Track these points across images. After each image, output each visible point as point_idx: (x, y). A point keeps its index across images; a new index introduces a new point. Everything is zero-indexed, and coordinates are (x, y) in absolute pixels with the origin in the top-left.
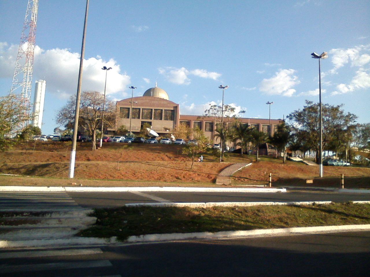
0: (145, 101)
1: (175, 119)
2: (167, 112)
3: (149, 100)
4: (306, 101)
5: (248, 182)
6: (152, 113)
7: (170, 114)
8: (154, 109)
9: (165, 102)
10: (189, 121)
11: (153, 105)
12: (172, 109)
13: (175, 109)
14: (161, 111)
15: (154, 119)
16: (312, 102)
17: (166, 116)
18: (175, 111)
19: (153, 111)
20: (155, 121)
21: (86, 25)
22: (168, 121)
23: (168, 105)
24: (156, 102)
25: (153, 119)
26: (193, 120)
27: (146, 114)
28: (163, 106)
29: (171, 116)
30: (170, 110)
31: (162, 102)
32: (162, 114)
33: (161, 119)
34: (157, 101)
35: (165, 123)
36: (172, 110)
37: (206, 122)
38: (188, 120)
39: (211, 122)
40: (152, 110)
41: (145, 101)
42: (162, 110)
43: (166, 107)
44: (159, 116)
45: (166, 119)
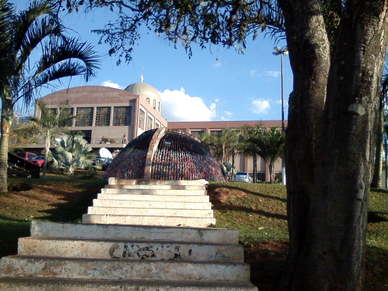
0: (82, 94)
1: (132, 123)
2: (119, 110)
3: (88, 92)
4: (190, 58)
5: (331, 21)
6: (92, 115)
7: (124, 115)
8: (97, 108)
9: (116, 94)
10: (203, 130)
11: (95, 100)
12: (127, 104)
13: (132, 104)
14: (108, 110)
15: (95, 124)
16: (192, 56)
17: (116, 118)
18: (133, 108)
19: (95, 111)
20: (98, 128)
21: (283, 96)
22: (120, 126)
23: (121, 98)
24: (100, 95)
25: (94, 125)
26: (209, 129)
27: (82, 118)
28: (112, 100)
29: (126, 118)
30: (123, 107)
31: (110, 94)
32: (110, 114)
33: (108, 124)
34: (102, 92)
35: (115, 131)
36: (126, 107)
37: (192, 130)
38: (201, 129)
39: (200, 130)
40: (109, 108)
41: (82, 94)
42: (109, 108)
43: (117, 102)
44: (105, 120)
45: (116, 124)
